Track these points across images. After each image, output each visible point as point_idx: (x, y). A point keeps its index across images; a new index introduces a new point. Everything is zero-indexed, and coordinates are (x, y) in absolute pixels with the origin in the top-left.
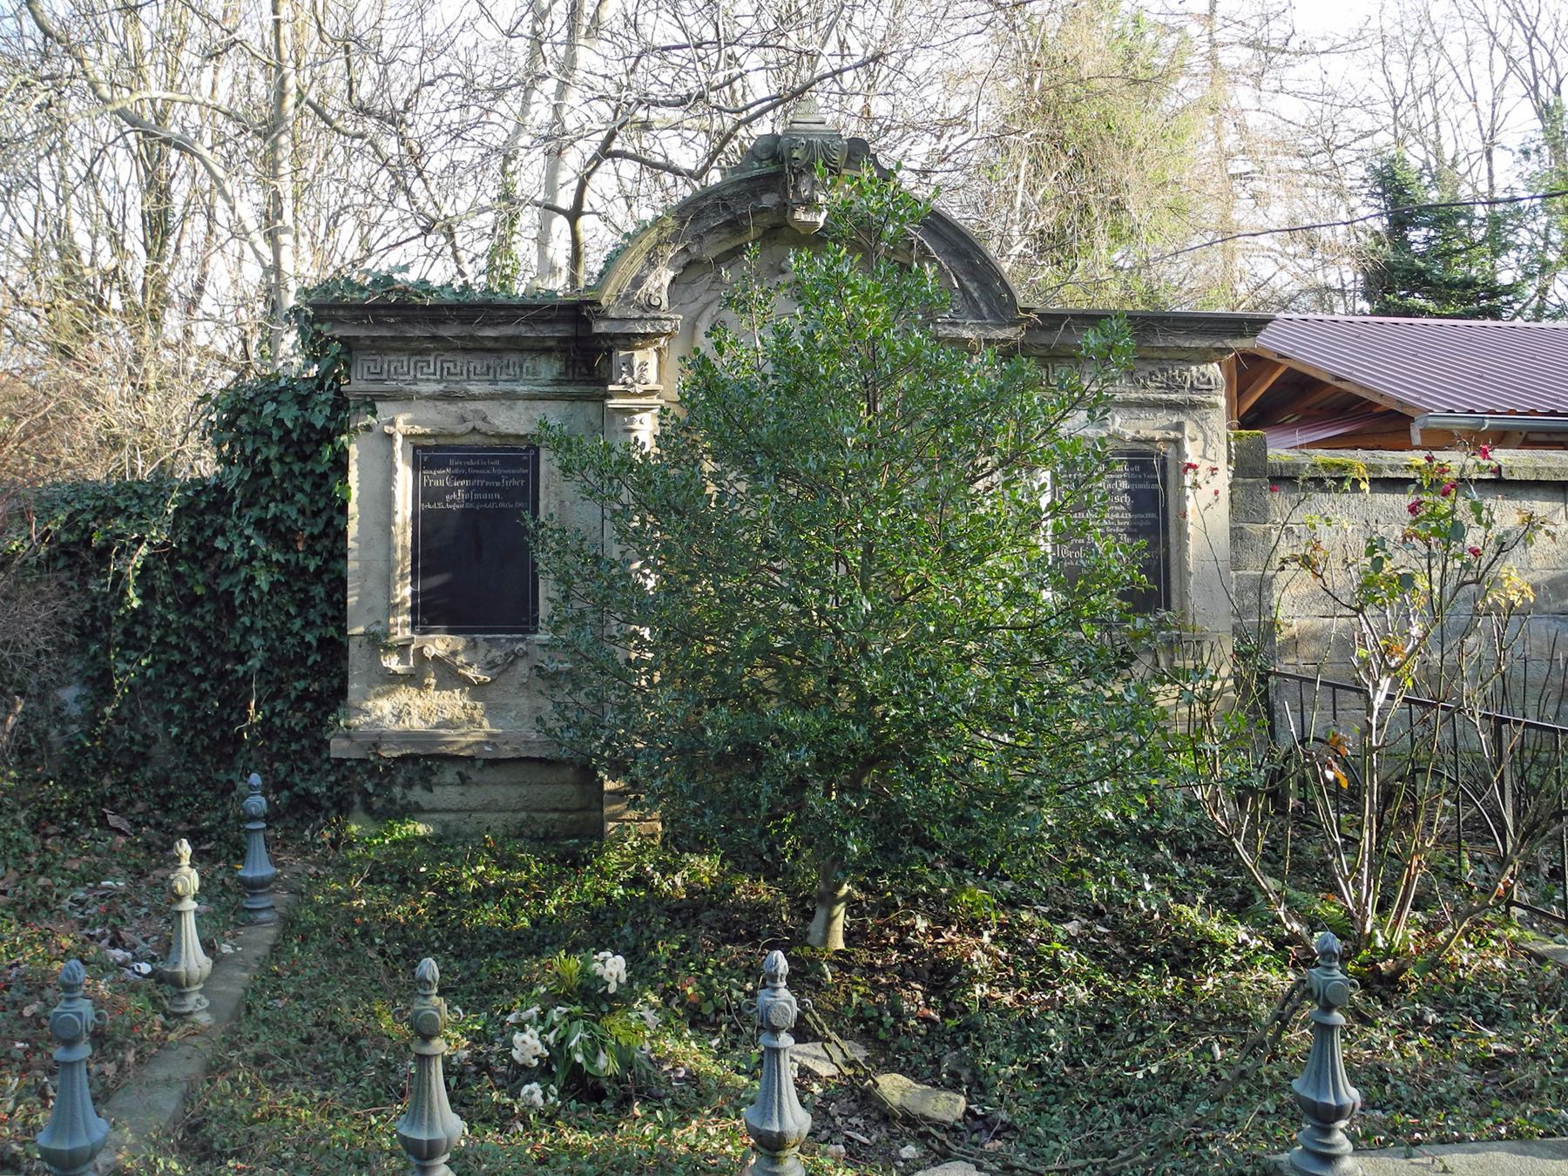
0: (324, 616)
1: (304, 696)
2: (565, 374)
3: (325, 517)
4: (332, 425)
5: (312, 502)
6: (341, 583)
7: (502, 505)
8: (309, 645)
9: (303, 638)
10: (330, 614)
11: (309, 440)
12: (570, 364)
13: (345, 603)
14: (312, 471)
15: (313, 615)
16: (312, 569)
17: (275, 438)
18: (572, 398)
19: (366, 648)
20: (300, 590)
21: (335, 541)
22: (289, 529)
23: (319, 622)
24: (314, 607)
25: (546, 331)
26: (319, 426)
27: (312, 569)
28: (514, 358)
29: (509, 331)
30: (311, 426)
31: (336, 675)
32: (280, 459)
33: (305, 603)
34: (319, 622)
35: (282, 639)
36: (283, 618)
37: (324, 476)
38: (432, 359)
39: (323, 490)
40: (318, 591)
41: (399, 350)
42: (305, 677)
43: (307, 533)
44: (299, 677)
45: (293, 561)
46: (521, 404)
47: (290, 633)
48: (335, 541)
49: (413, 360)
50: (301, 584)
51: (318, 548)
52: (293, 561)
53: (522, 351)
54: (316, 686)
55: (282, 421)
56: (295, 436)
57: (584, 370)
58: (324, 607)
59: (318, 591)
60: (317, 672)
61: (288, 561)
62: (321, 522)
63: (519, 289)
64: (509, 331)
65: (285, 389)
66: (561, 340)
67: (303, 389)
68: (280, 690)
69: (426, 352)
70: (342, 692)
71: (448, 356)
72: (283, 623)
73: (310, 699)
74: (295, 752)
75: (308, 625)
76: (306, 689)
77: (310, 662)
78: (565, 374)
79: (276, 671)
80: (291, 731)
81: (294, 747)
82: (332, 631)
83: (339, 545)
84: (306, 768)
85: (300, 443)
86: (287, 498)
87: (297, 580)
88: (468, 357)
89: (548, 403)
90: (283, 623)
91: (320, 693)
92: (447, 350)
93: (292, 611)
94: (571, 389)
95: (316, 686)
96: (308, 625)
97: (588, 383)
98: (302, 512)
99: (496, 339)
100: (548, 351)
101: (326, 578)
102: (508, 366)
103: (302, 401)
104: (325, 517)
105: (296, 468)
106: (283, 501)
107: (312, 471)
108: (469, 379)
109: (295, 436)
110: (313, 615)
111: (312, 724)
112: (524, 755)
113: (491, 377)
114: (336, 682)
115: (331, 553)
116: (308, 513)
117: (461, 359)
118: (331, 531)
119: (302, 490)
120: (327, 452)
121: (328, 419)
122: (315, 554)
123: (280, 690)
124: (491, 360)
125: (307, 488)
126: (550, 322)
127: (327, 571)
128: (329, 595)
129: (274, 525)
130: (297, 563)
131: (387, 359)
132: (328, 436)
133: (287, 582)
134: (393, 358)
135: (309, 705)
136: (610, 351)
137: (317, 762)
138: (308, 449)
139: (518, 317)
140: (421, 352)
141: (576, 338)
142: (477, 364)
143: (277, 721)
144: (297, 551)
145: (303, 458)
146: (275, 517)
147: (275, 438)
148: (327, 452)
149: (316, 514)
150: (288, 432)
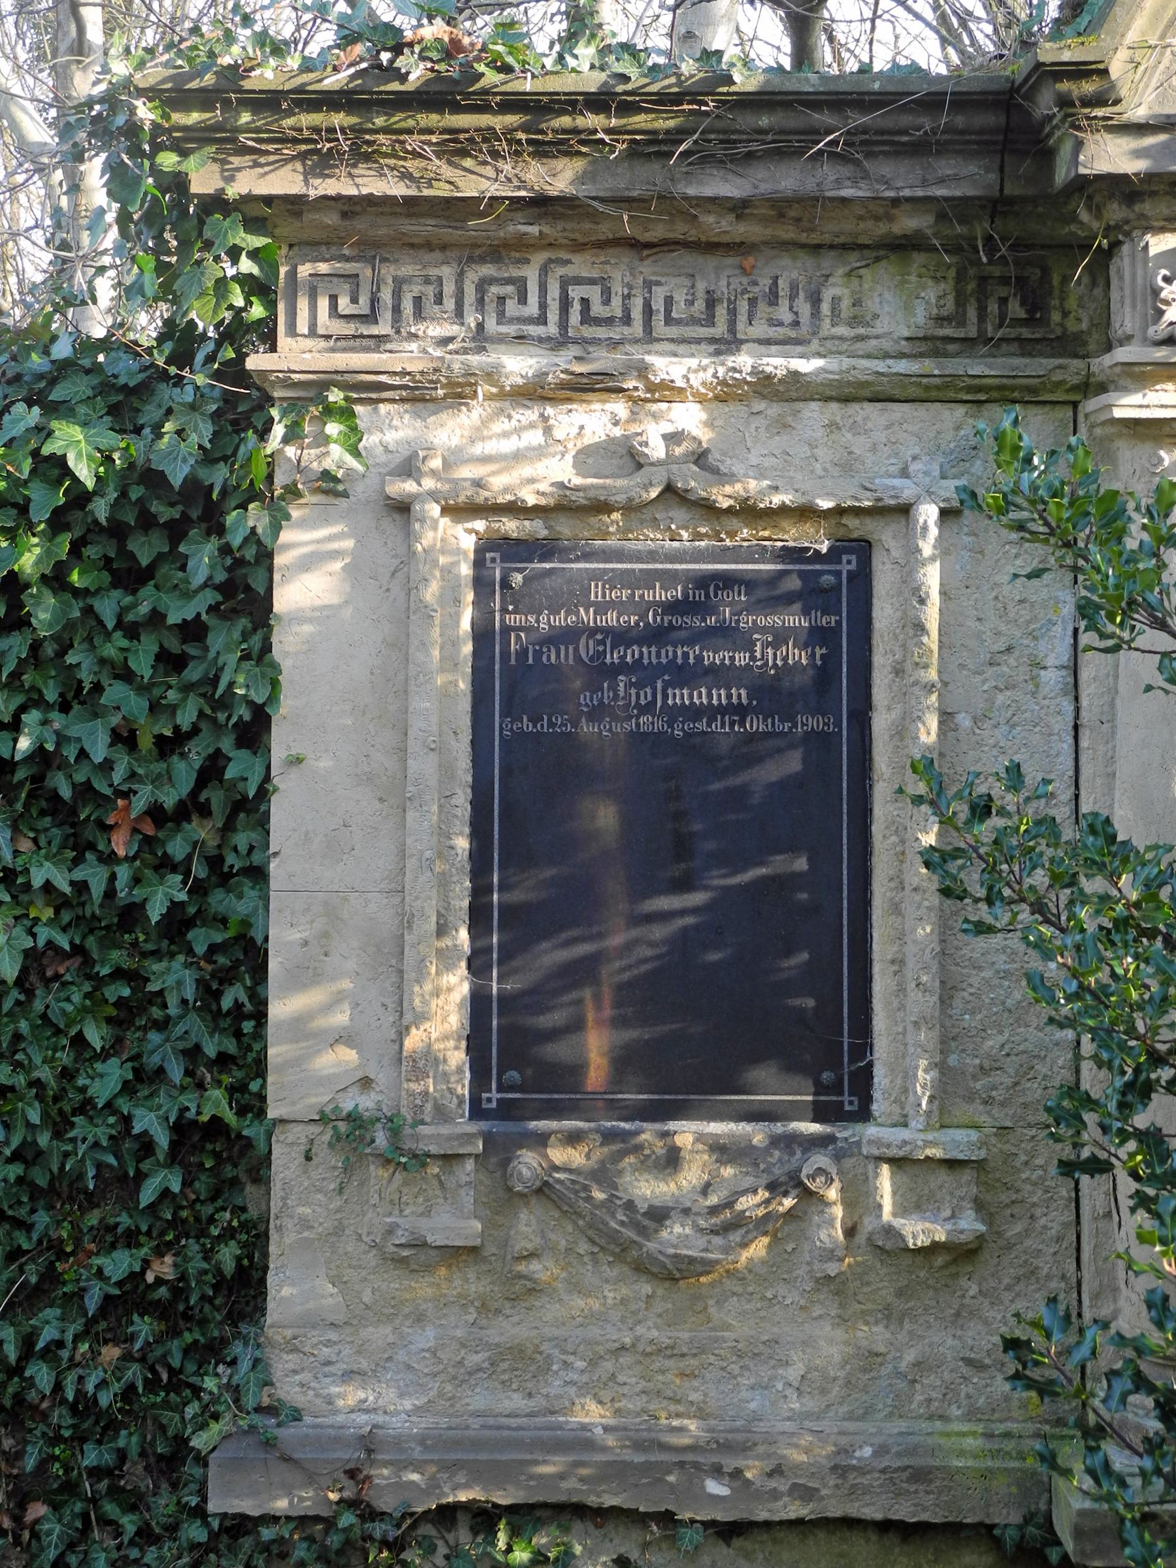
0: (193, 1053)
1: (131, 1296)
2: (958, 318)
3: (197, 753)
4: (218, 476)
5: (155, 708)
6: (249, 956)
7: (754, 724)
8: (146, 1145)
9: (127, 1120)
10: (211, 1050)
11: (147, 522)
12: (973, 286)
13: (261, 1016)
14: (156, 618)
15: (159, 1049)
16: (155, 913)
17: (40, 515)
18: (979, 395)
19: (329, 1160)
20: (119, 974)
21: (229, 827)
22: (85, 791)
23: (176, 1073)
24: (163, 1025)
25: (901, 178)
26: (177, 476)
27: (155, 913)
28: (790, 271)
29: (787, 179)
30: (154, 479)
31: (229, 1233)
32: (56, 580)
33: (133, 1014)
34: (176, 1073)
35: (60, 1126)
36: (65, 1058)
37: (194, 631)
38: (531, 274)
39: (193, 673)
40: (175, 978)
41: (429, 246)
42: (131, 1239)
43: (139, 804)
44: (112, 1238)
45: (97, 889)
46: (814, 414)
47: (86, 1107)
48: (229, 827)
49: (472, 277)
50: (118, 957)
51: (177, 848)
52: (97, 889)
53: (816, 249)
54: (165, 1267)
55: (60, 462)
56: (101, 509)
57: (1016, 309)
58: (194, 1027)
59: (175, 978)
60: (174, 1226)
61: (81, 887)
62: (185, 770)
63: (462, 499)
64: (787, 179)
65: (64, 368)
66: (946, 210)
67: (126, 370)
68: (50, 1277)
69: (520, 248)
70: (245, 1289)
71: (581, 265)
72: (67, 1075)
73: (147, 1307)
74: (96, 1473)
75: (143, 1078)
76: (135, 1277)
77: (147, 1196)
78: (958, 318)
79: (42, 1219)
80: (83, 1406)
81: (91, 1456)
82: (216, 1103)
83: (241, 839)
84: (129, 1524)
85: (117, 531)
86: (77, 697)
87: (109, 943)
88: (647, 269)
89: (898, 411)
90: (67, 1075)
91: (179, 1288)
92: (578, 247)
93: (95, 1036)
94: (977, 367)
95: (165, 1267)
96: (143, 1078)
97: (1027, 347)
98: (125, 738)
99: (739, 208)
100: (902, 247)
101: (200, 939)
102: (773, 298)
103: (124, 402)
104: (197, 753)
105: (107, 608)
106: (65, 707)
107: (156, 618)
108: (649, 337)
109: (101, 509)
110: (159, 1049)
111: (152, 1384)
112: (835, 1511)
113: (720, 329)
114: (228, 1255)
115: (215, 862)
116: (146, 742)
117: (621, 272)
118: (215, 797)
119: (126, 675)
120: (203, 559)
121: (208, 458)
122: (165, 865)
123: (50, 1277)
124: (721, 277)
125: (142, 664)
126: (919, 149)
127: (202, 917)
128: (209, 992)
129: (37, 779)
130: (110, 893)
131: (388, 272)
132: (204, 509)
133: (78, 950)
134: (407, 270)
135: (144, 1327)
136: (1119, 236)
137: (164, 1504)
138: (144, 550)
139: (816, 133)
140: (496, 252)
141: (997, 206)
142: (674, 287)
143: (42, 1375)
144: (109, 859)
145: (130, 577)
146: (39, 754)
147: (40, 515)
148: (203, 559)
149: (168, 746)
150: (80, 498)
